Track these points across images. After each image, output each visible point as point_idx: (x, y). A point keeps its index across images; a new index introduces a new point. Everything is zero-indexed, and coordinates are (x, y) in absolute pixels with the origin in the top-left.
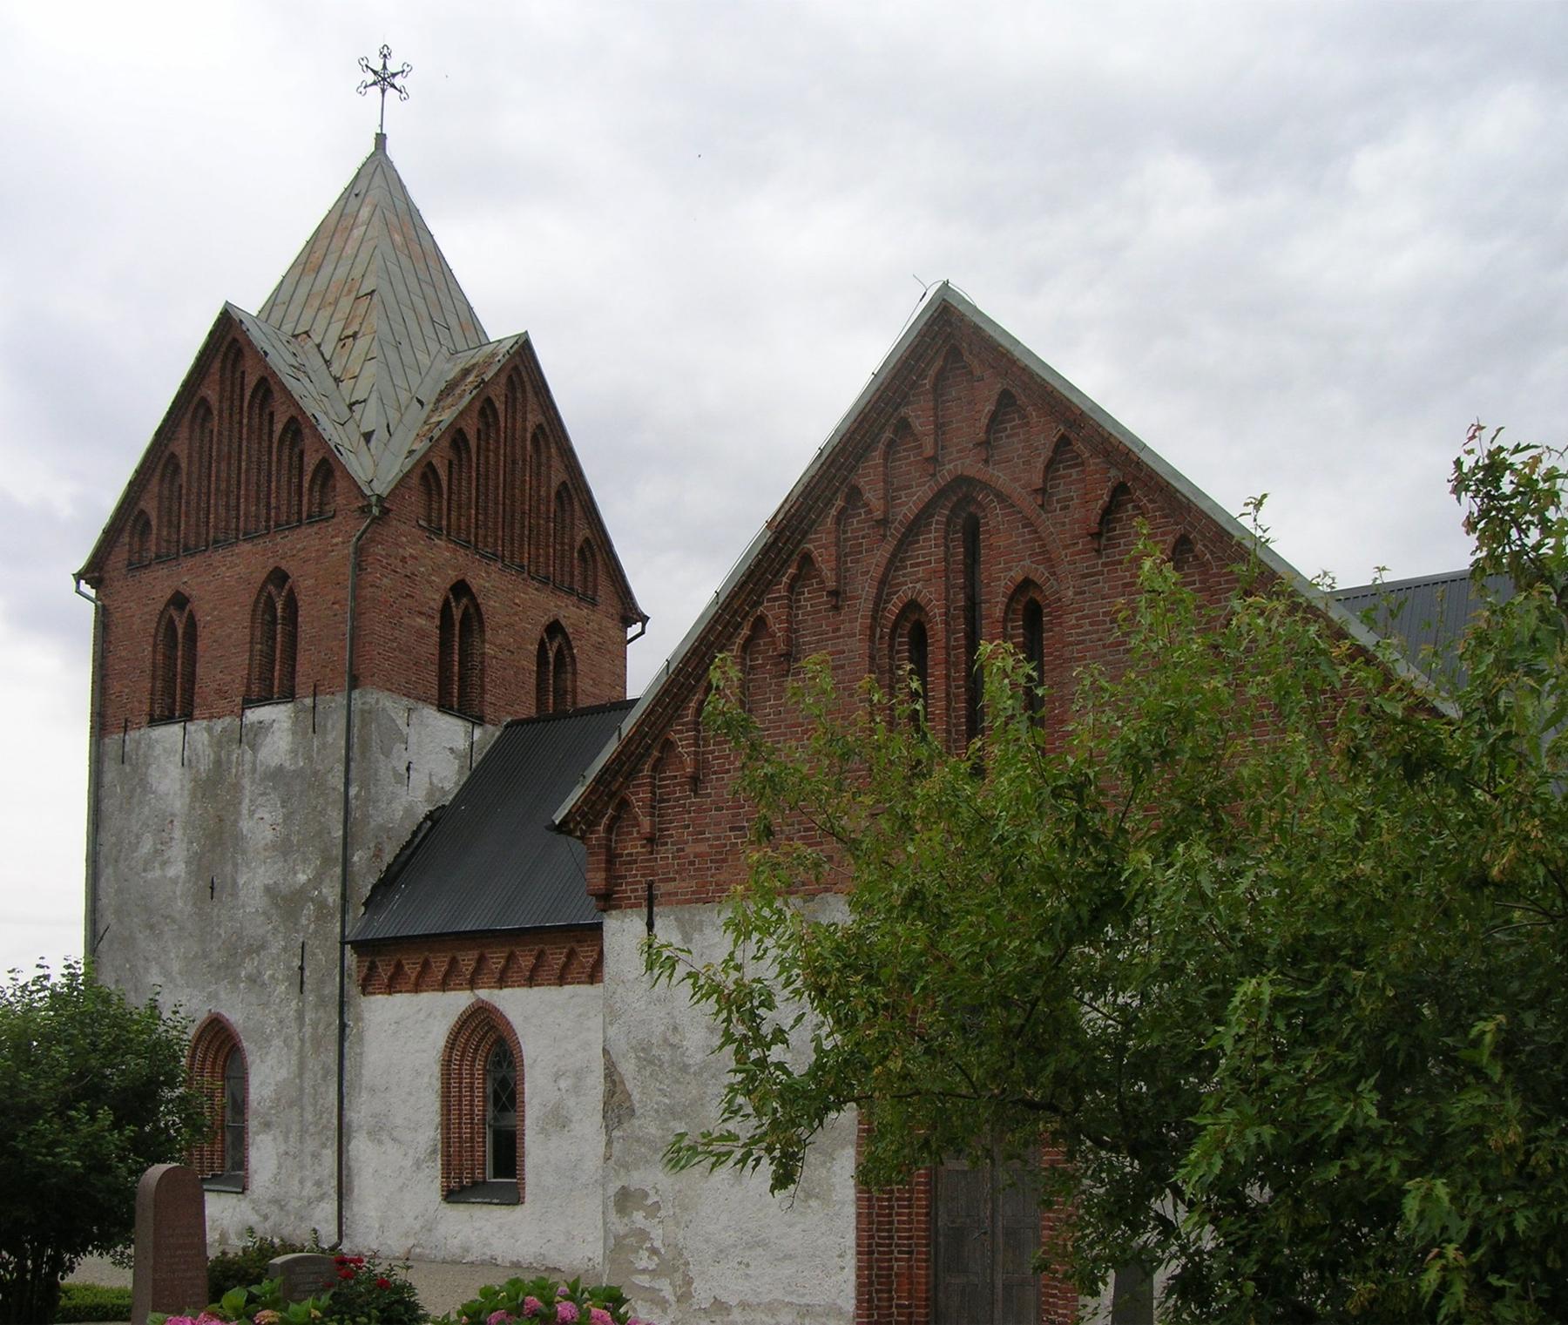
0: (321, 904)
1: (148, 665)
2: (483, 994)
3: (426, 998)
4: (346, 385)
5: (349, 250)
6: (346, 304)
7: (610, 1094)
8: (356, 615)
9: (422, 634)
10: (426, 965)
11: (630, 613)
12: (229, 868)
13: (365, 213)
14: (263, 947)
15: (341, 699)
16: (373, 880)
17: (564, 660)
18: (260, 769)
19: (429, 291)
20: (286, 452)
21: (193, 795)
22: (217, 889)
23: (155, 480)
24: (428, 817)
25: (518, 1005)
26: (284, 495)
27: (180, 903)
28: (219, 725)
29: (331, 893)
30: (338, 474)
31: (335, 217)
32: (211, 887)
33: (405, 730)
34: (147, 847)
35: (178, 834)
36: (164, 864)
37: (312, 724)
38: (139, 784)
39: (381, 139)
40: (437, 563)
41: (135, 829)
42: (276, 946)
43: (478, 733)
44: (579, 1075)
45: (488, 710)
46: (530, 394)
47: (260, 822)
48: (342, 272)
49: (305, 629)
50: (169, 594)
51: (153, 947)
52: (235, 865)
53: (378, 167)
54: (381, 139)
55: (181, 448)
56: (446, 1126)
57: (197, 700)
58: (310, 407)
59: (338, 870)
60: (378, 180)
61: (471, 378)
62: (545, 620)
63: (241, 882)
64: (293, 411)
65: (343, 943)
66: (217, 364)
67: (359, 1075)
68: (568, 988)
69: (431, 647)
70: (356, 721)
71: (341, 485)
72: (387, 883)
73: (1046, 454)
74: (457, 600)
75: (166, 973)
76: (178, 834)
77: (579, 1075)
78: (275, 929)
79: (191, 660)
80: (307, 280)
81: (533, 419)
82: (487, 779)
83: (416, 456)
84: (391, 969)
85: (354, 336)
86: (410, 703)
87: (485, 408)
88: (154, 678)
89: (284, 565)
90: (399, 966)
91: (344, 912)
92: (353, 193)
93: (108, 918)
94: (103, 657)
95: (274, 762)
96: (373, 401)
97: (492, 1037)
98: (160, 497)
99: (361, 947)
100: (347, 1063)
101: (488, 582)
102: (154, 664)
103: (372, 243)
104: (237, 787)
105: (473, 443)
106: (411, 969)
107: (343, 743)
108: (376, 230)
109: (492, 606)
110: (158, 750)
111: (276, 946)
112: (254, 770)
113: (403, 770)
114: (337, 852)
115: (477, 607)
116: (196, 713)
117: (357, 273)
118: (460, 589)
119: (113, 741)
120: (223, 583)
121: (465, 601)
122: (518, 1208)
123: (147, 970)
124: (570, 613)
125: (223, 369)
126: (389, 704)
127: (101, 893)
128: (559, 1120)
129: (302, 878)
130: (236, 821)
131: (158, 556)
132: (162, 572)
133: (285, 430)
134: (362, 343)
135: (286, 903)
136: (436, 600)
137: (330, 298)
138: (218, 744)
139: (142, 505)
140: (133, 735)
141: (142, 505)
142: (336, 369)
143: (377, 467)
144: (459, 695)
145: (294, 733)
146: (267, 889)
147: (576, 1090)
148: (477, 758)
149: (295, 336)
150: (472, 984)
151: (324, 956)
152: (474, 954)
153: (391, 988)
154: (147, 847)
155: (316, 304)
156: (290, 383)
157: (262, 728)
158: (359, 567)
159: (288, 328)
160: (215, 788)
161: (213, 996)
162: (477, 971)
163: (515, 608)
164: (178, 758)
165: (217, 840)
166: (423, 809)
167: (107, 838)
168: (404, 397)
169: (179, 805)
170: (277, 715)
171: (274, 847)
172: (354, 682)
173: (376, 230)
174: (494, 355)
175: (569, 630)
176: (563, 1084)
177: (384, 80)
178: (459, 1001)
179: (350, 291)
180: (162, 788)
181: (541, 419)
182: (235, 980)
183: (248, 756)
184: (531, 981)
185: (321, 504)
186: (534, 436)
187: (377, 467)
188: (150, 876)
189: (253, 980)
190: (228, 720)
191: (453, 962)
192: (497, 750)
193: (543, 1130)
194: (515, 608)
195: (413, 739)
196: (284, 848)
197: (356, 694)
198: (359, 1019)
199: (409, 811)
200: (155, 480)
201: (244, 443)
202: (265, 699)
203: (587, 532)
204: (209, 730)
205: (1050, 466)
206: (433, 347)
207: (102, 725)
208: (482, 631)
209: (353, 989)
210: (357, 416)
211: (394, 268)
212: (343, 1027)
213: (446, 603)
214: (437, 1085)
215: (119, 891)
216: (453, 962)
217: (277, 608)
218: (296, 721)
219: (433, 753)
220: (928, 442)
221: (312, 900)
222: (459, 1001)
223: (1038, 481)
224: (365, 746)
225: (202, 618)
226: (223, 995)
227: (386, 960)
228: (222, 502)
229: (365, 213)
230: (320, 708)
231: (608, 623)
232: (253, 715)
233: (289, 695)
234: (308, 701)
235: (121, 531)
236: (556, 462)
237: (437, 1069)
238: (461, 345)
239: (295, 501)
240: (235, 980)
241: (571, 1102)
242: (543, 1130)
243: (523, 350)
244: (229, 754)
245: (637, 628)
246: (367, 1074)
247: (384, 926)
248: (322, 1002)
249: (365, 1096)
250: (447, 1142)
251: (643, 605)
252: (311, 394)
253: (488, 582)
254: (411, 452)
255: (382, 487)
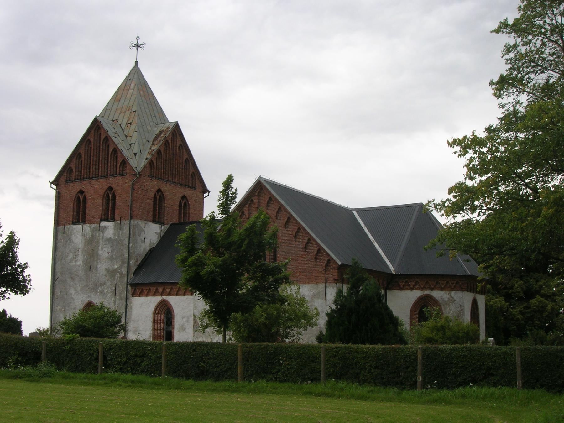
0: (121, 274)
1: (72, 208)
2: (164, 297)
3: (149, 298)
4: (129, 138)
5: (128, 97)
6: (128, 113)
7: (195, 323)
8: (132, 201)
9: (149, 204)
10: (149, 290)
11: (205, 190)
12: (95, 263)
13: (132, 86)
14: (105, 284)
15: (128, 222)
16: (135, 268)
17: (186, 205)
18: (105, 238)
19: (150, 106)
20: (113, 156)
21: (85, 243)
22: (92, 268)
23: (74, 159)
24: (150, 250)
25: (173, 300)
26: (112, 167)
27: (80, 272)
28: (93, 226)
29: (124, 271)
30: (127, 164)
31: (124, 85)
32: (90, 268)
33: (144, 229)
34: (71, 256)
35: (80, 253)
36: (76, 261)
37: (119, 227)
38: (69, 240)
39: (136, 63)
40: (153, 185)
41: (67, 251)
42: (108, 284)
43: (163, 227)
44: (188, 318)
45: (166, 221)
46: (178, 137)
47: (104, 252)
48: (126, 103)
49: (118, 202)
50: (78, 190)
51: (72, 283)
52: (97, 262)
53: (136, 74)
54: (136, 63)
55: (82, 152)
56: (154, 330)
57: (87, 219)
58: (120, 147)
59: (126, 265)
60: (136, 76)
61: (162, 135)
62: (181, 196)
63: (99, 266)
64: (115, 146)
65: (127, 284)
66: (93, 131)
67: (131, 317)
68: (186, 297)
69: (151, 207)
70: (132, 227)
71: (128, 167)
72: (139, 268)
73: (277, 210)
74: (158, 193)
75: (76, 290)
76: (80, 253)
77: (188, 318)
78: (108, 279)
79: (85, 208)
80: (116, 103)
81: (179, 143)
82: (166, 240)
83: (148, 160)
84: (140, 291)
85: (131, 123)
86: (144, 222)
87: (166, 142)
88: (73, 212)
89: (112, 186)
90: (142, 290)
91: (128, 276)
92: (128, 79)
93: (58, 275)
94: (58, 205)
95: (109, 236)
96: (136, 144)
97: (166, 308)
98: (76, 164)
99: (132, 285)
100: (127, 314)
101: (167, 188)
102: (74, 208)
103: (135, 96)
104: (98, 242)
105: (163, 153)
106: (146, 291)
107: (128, 233)
108: (136, 88)
109: (167, 194)
110: (75, 231)
111: (108, 284)
112: (103, 238)
113: (143, 239)
114: (126, 260)
115: (163, 195)
116: (86, 222)
117: (131, 104)
118: (159, 191)
119: (61, 228)
120: (94, 189)
121: (160, 193)
122: (497, 34)
123: (70, 289)
124: (188, 192)
125: (94, 133)
126: (140, 223)
127: (56, 269)
128: (183, 328)
129: (116, 267)
130: (97, 252)
131: (75, 180)
132: (77, 184)
133: (113, 150)
134: (133, 126)
135: (111, 273)
136: (152, 195)
137: (123, 111)
138: (93, 230)
139: (70, 165)
140: (67, 227)
141: (70, 165)
142: (126, 132)
143: (138, 163)
144: (157, 219)
145: (114, 229)
146: (106, 269)
147: (187, 321)
148: (163, 234)
149: (113, 121)
150: (162, 295)
151: (122, 287)
152: (162, 288)
153: (140, 295)
154: (71, 256)
155: (119, 112)
156: (114, 139)
157: (105, 228)
158: (133, 188)
159: (111, 118)
160: (91, 243)
161: (90, 296)
162: (163, 292)
163: (173, 193)
164: (81, 234)
165: (92, 256)
166: (148, 248)
167: (59, 254)
168: (144, 141)
169: (81, 246)
170: (110, 225)
171: (108, 258)
172: (131, 218)
173: (136, 88)
174: (168, 128)
175: (188, 197)
176: (184, 320)
177: (137, 46)
178: (158, 299)
179: (129, 110)
180: (76, 241)
181: (181, 142)
182: (96, 292)
183: (101, 234)
184: (177, 294)
185: (123, 171)
186: (179, 147)
187: (138, 163)
188: (71, 264)
189: (101, 292)
190: (96, 225)
191: (157, 289)
192: (168, 232)
193: (179, 331)
194: (173, 193)
195: (146, 231)
196: (111, 259)
197: (132, 221)
198: (131, 303)
199: (145, 249)
200: (74, 159)
201: (101, 153)
202: (107, 220)
203: (193, 170)
204: (90, 227)
205: (278, 212)
206: (151, 123)
207: (58, 222)
208: (164, 201)
209: (130, 295)
210: (132, 148)
211: (141, 103)
212: (127, 305)
213: (155, 195)
214: (152, 320)
215: (62, 268)
216: (157, 289)
217: (110, 197)
218: (115, 226)
219: (152, 233)
220: (257, 204)
221: (119, 272)
222: (158, 299)
223: (275, 214)
224: (134, 234)
225: (89, 197)
226: (92, 296)
227: (139, 288)
228: (94, 167)
229: (132, 86)
230: (122, 223)
231: (198, 194)
232: (103, 224)
233: (113, 219)
234: (119, 222)
235: (64, 172)
236: (185, 153)
237: (152, 316)
238: (159, 121)
239: (115, 169)
240: (96, 292)
241: (186, 324)
242: (179, 331)
243: (177, 126)
244: (96, 234)
245: (207, 194)
246: (133, 317)
247: (139, 280)
248: (121, 298)
249: (132, 322)
250: (154, 334)
251: (209, 188)
252: (119, 141)
253: (167, 188)
254: (147, 158)
255: (139, 169)
